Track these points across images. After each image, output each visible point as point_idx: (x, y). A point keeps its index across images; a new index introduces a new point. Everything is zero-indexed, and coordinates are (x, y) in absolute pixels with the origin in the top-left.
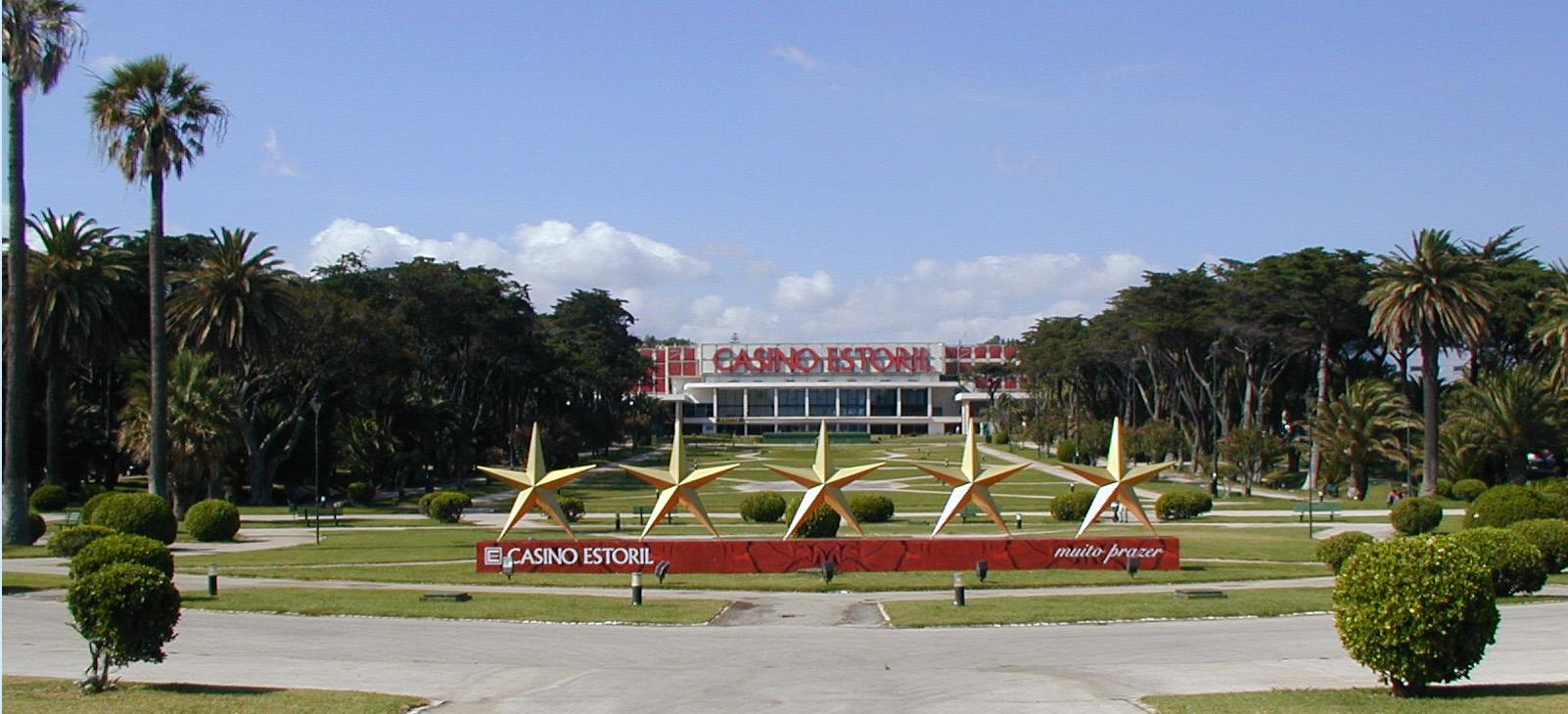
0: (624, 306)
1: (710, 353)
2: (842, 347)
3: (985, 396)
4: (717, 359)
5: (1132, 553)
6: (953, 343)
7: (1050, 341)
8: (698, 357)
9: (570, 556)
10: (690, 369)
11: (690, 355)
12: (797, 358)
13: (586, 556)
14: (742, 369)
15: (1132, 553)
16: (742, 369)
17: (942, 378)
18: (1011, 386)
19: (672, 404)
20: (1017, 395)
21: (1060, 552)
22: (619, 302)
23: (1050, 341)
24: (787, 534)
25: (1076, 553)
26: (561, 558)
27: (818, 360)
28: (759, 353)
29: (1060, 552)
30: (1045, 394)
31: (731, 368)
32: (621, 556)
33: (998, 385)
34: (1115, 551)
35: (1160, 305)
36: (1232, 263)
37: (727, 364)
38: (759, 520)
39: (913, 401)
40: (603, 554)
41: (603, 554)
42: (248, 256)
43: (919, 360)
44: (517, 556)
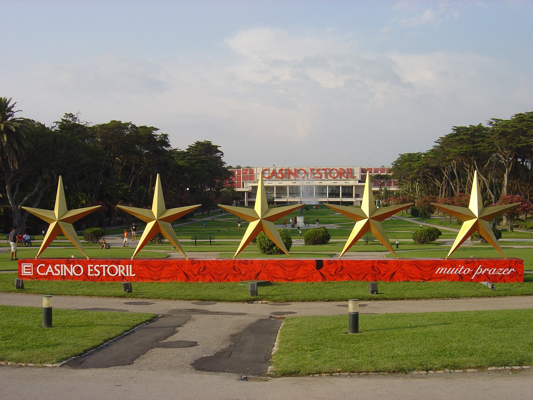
0: (219, 149)
1: (260, 171)
2: (317, 168)
3: (377, 189)
4: (263, 173)
5: (492, 271)
6: (365, 167)
7: (407, 163)
8: (255, 172)
9: (78, 270)
10: (251, 177)
11: (252, 171)
12: (297, 172)
13: (89, 270)
14: (274, 178)
15: (492, 271)
16: (274, 178)
17: (359, 182)
18: (389, 185)
19: (243, 193)
20: (392, 189)
21: (440, 270)
22: (217, 147)
23: (407, 163)
24: (46, 274)
25: (452, 271)
26: (72, 271)
27: (305, 172)
28: (281, 170)
29: (440, 270)
30: (407, 186)
31: (269, 178)
32: (113, 271)
33: (383, 183)
34: (480, 271)
35: (461, 141)
36: (497, 120)
37: (267, 176)
38: (315, 243)
39: (347, 192)
40: (101, 269)
41: (101, 269)
42: (9, 106)
43: (350, 173)
44: (43, 270)
